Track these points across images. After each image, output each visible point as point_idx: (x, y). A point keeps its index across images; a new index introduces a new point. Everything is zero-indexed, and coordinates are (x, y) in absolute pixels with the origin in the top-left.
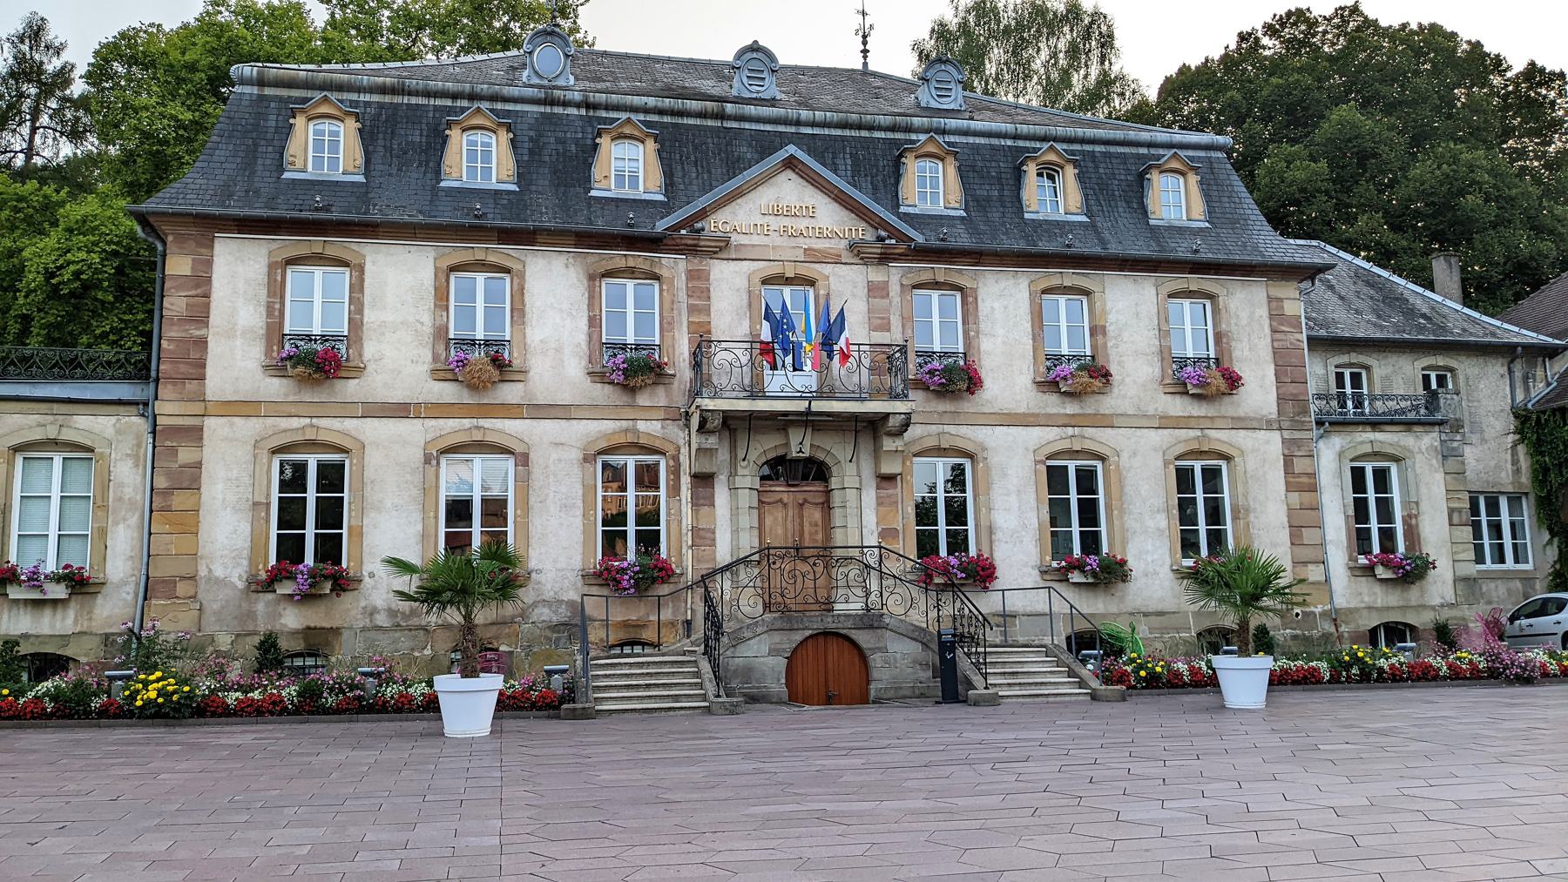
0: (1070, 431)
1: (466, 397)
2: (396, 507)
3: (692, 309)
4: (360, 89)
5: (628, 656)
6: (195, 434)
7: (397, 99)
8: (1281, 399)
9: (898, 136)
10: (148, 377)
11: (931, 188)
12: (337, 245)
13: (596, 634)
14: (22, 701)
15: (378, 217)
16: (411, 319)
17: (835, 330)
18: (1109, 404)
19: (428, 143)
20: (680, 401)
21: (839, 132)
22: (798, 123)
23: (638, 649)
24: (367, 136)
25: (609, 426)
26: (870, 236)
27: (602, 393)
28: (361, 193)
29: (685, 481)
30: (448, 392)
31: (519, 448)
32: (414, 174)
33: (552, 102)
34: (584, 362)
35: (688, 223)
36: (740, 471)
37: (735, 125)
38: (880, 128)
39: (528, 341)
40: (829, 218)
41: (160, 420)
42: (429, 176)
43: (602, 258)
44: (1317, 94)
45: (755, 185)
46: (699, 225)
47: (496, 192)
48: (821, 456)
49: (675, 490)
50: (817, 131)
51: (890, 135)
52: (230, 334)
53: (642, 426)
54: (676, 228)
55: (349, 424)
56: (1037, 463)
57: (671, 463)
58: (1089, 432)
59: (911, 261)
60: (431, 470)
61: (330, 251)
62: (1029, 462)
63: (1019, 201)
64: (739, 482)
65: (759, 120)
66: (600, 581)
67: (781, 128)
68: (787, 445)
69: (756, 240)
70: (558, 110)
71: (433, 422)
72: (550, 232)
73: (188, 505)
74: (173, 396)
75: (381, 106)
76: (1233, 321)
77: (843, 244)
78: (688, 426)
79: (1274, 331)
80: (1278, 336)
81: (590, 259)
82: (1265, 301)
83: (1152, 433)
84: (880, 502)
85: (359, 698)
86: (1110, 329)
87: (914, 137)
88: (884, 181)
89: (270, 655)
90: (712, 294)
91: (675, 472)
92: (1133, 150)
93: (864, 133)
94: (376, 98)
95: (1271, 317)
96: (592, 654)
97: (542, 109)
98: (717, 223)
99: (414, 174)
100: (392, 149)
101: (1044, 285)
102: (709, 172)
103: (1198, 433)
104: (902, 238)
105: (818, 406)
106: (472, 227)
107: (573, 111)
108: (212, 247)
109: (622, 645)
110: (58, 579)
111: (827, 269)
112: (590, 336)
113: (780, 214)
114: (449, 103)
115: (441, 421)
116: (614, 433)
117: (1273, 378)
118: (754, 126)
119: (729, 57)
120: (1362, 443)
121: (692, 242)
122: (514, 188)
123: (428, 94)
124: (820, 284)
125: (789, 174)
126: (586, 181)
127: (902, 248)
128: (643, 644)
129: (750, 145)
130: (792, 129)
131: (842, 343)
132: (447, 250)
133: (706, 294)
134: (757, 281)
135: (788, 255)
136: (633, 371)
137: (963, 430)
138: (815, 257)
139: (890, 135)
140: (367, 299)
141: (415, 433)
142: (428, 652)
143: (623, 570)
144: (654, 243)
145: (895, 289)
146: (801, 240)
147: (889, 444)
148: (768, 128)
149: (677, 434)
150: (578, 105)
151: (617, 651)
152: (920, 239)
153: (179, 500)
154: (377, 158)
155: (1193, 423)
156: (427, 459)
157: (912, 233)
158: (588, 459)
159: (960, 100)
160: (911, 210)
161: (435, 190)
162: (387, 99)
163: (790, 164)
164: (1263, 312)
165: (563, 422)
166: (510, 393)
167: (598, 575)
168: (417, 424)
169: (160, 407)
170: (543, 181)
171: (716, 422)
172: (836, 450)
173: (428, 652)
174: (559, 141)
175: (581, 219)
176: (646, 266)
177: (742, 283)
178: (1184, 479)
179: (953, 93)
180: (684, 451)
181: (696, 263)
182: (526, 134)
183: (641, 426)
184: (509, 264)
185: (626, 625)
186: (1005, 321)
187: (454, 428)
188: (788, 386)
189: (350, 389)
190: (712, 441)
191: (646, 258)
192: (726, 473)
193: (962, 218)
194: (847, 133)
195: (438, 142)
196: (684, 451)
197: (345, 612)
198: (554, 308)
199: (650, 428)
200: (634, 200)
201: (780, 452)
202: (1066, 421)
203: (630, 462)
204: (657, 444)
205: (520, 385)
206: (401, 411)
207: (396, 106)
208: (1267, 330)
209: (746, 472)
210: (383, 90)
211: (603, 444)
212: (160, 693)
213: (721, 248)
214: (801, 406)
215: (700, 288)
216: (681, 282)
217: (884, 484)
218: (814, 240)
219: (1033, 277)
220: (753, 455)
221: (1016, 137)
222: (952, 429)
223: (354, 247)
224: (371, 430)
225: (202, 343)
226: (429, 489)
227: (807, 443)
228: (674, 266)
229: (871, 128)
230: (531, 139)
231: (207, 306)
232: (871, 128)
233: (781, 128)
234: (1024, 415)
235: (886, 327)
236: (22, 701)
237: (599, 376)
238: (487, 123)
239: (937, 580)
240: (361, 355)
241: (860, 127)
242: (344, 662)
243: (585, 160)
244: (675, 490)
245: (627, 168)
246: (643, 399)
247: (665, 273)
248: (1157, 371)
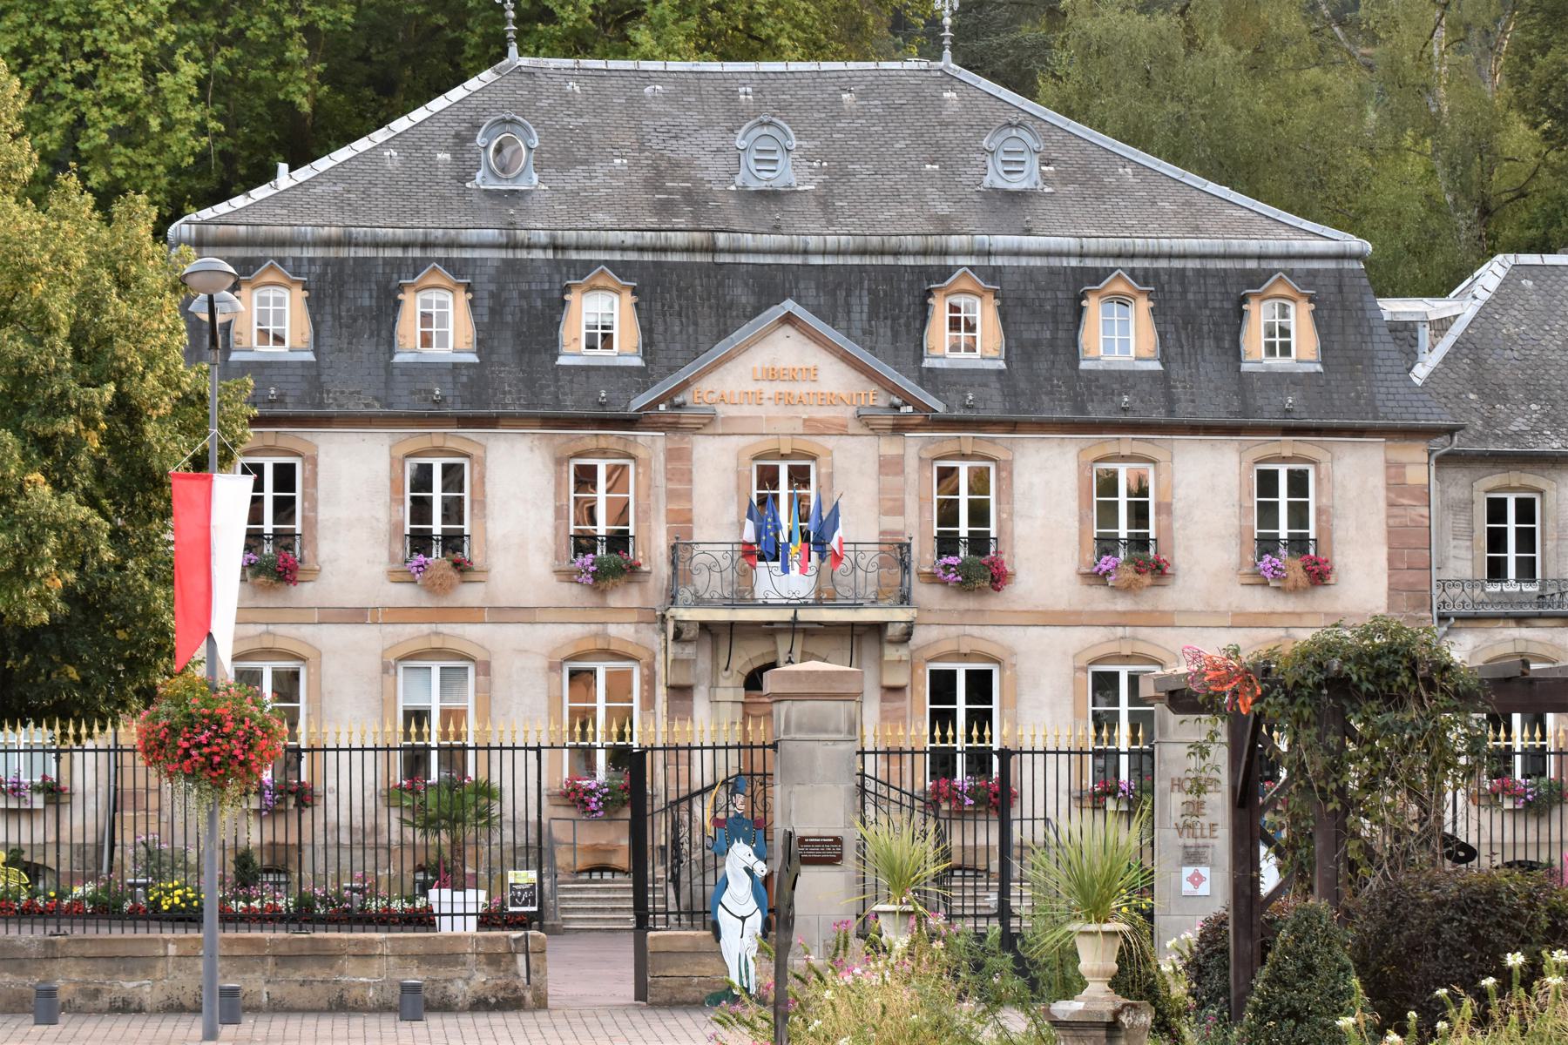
0: (1120, 631)
1: (425, 601)
3: (672, 495)
4: (303, 244)
5: (596, 882)
7: (344, 253)
8: (1393, 589)
9: (931, 261)
11: (967, 336)
13: (563, 858)
14: (66, 902)
15: (333, 410)
17: (826, 531)
18: (1168, 598)
19: (379, 308)
20: (657, 601)
21: (856, 260)
22: (806, 252)
23: (607, 876)
24: (315, 304)
25: (576, 630)
26: (882, 401)
27: (570, 593)
28: (312, 375)
29: (661, 692)
30: (405, 595)
31: (480, 656)
32: (366, 346)
33: (513, 245)
34: (550, 558)
35: (667, 397)
36: (722, 682)
37: (728, 259)
38: (907, 253)
39: (490, 536)
40: (834, 378)
42: (382, 348)
43: (571, 438)
45: (746, 347)
46: (678, 400)
47: (456, 366)
49: (649, 702)
50: (829, 260)
51: (921, 261)
53: (613, 630)
54: (654, 405)
55: (306, 631)
56: (1077, 669)
57: (646, 672)
58: (1144, 632)
59: (932, 431)
60: (389, 679)
62: (1067, 669)
63: (1076, 345)
64: (721, 694)
65: (757, 251)
66: (567, 801)
67: (785, 260)
68: (775, 652)
69: (747, 410)
70: (522, 254)
71: (390, 628)
72: (512, 417)
74: (201, 652)
75: (326, 262)
76: (1337, 494)
77: (850, 412)
78: (664, 631)
79: (1391, 505)
80: (1395, 511)
81: (558, 441)
82: (1381, 466)
83: (1223, 632)
84: (884, 716)
85: (347, 910)
86: (1178, 506)
87: (950, 261)
88: (908, 325)
89: (246, 870)
90: (696, 476)
91: (649, 682)
92: (1238, 265)
93: (889, 260)
94: (320, 253)
95: (1389, 487)
96: (560, 878)
97: (503, 254)
99: (366, 346)
100: (340, 317)
102: (696, 324)
103: (1282, 632)
104: (919, 406)
105: (805, 615)
106: (430, 416)
107: (538, 254)
109: (590, 871)
110: (35, 789)
111: (830, 442)
112: (556, 528)
113: (779, 377)
114: (399, 253)
115: (399, 627)
116: (582, 638)
117: (1385, 564)
118: (752, 259)
120: (1503, 641)
121: (674, 419)
122: (473, 358)
123: (376, 245)
124: (821, 459)
125: (788, 330)
126: (552, 345)
127: (918, 419)
128: (614, 871)
129: (747, 285)
130: (798, 260)
131: (834, 544)
132: (403, 437)
133: (687, 476)
134: (746, 458)
135: (785, 427)
136: (603, 559)
137: (989, 632)
138: (816, 428)
139: (921, 261)
140: (321, 495)
141: (370, 640)
143: (591, 792)
144: (629, 423)
145: (911, 464)
146: (800, 408)
147: (891, 653)
148: (769, 260)
149: (653, 639)
150: (544, 248)
151: (585, 876)
152: (940, 408)
154: (328, 341)
156: (386, 669)
158: (554, 667)
159: (1036, 176)
160: (937, 364)
161: (389, 367)
162: (332, 253)
163: (789, 319)
164: (1378, 481)
165: (527, 627)
166: (470, 595)
167: (566, 795)
170: (506, 348)
171: (693, 632)
174: (524, 295)
175: (547, 398)
176: (619, 447)
177: (729, 462)
179: (1026, 168)
180: (660, 658)
181: (676, 440)
182: (486, 287)
183: (613, 630)
184: (468, 450)
185: (594, 849)
186: (1044, 492)
187: (412, 634)
188: (784, 586)
189: (305, 593)
190: (688, 651)
191: (619, 437)
192: (707, 683)
193: (1000, 372)
194: (867, 260)
195: (389, 307)
196: (660, 658)
197: (314, 825)
198: (518, 490)
199: (622, 632)
200: (608, 368)
202: (1115, 620)
203: (602, 669)
204: (630, 650)
205: (480, 587)
206: (357, 616)
207: (341, 262)
208: (1382, 504)
209: (729, 683)
210: (327, 243)
211: (571, 651)
212: (183, 899)
213: (707, 423)
214: (786, 615)
215: (679, 463)
216: (659, 463)
217: (891, 696)
218: (815, 408)
219: (1083, 444)
221: (1082, 255)
222: (975, 631)
223: (307, 437)
224: (331, 637)
226: (387, 701)
228: (652, 444)
229: (896, 253)
230: (492, 295)
232: (896, 253)
233: (785, 260)
234: (1064, 613)
235: (899, 510)
236: (66, 902)
237: (568, 576)
238: (445, 284)
239: (945, 807)
240: (316, 556)
241: (882, 253)
242: (320, 875)
243: (552, 318)
244: (649, 702)
245: (600, 322)
246: (615, 600)
247: (641, 453)
248: (1234, 558)
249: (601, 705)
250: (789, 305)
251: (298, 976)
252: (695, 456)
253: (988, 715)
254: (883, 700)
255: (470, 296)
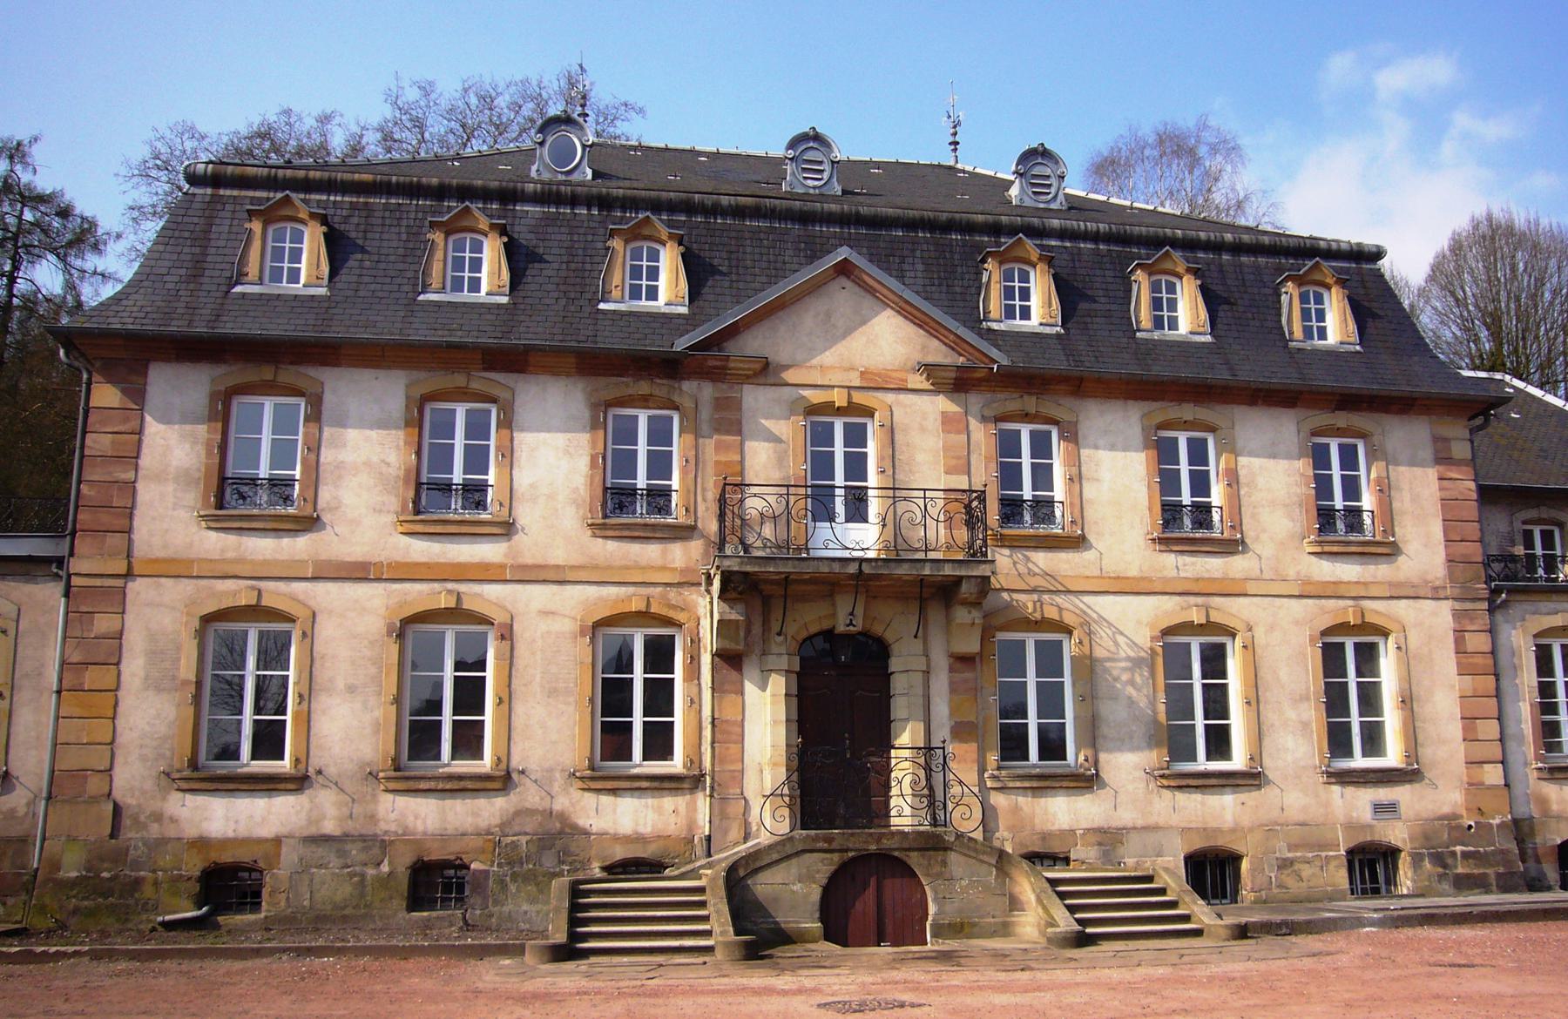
2: (351, 689)
6: (118, 600)
8: (1450, 560)
10: (64, 528)
12: (288, 375)
16: (375, 459)
31: (499, 617)
36: (775, 649)
41: (75, 581)
44: (1169, 182)
48: (878, 629)
52: (159, 477)
61: (475, 385)
68: (834, 615)
73: (109, 682)
98: (754, 344)
101: (1159, 419)
108: (145, 375)
119: (778, 150)
125: (843, 281)
142: (385, 868)
153: (92, 677)
155: (1342, 591)
157: (994, 353)
163: (844, 269)
165: (555, 588)
168: (378, 588)
169: (76, 565)
172: (897, 627)
173: (385, 868)
178: (1332, 657)
193: (1058, 335)
201: (826, 625)
206: (359, 572)
220: (791, 629)
225: (130, 488)
227: (859, 611)
231: (140, 441)
247: (688, 403)
249: (839, 479)
250: (843, 253)
251: (851, 854)
252: (745, 406)
253: (1004, 714)
254: (951, 670)
255: (505, 239)
